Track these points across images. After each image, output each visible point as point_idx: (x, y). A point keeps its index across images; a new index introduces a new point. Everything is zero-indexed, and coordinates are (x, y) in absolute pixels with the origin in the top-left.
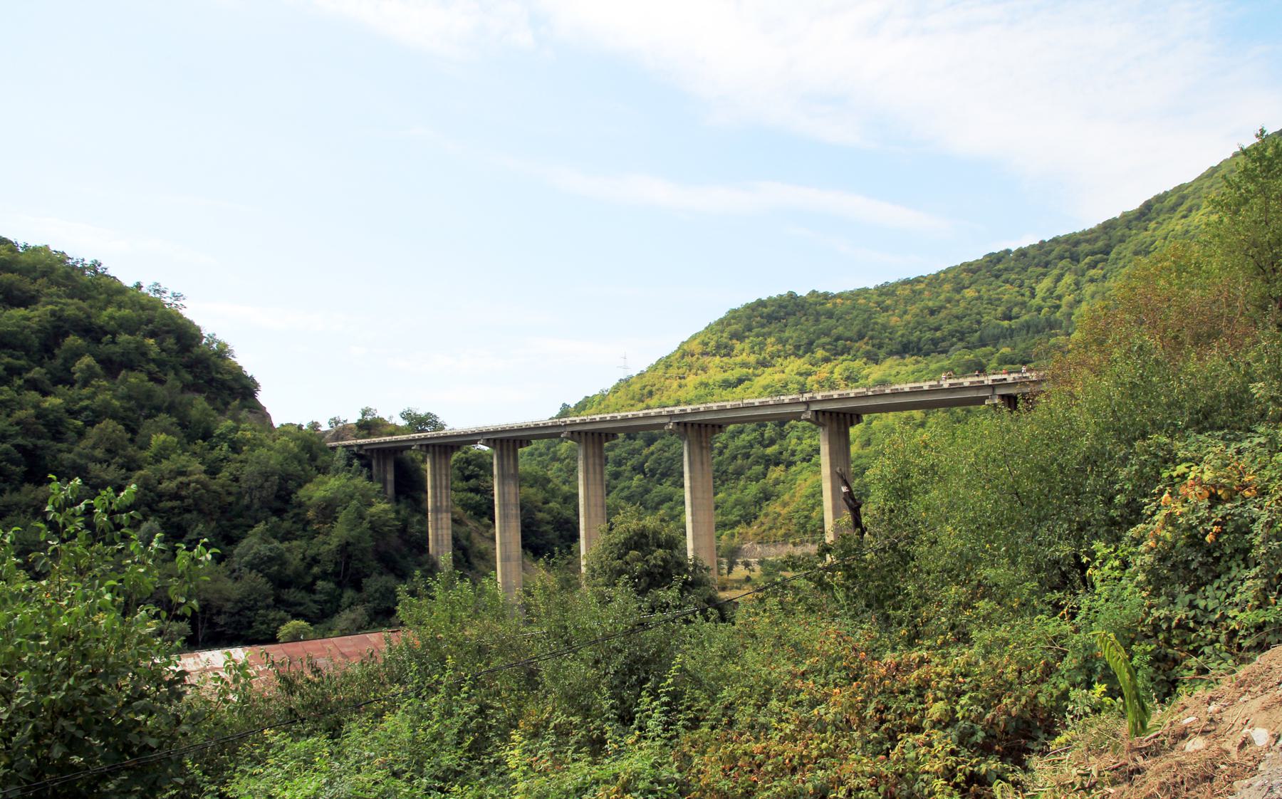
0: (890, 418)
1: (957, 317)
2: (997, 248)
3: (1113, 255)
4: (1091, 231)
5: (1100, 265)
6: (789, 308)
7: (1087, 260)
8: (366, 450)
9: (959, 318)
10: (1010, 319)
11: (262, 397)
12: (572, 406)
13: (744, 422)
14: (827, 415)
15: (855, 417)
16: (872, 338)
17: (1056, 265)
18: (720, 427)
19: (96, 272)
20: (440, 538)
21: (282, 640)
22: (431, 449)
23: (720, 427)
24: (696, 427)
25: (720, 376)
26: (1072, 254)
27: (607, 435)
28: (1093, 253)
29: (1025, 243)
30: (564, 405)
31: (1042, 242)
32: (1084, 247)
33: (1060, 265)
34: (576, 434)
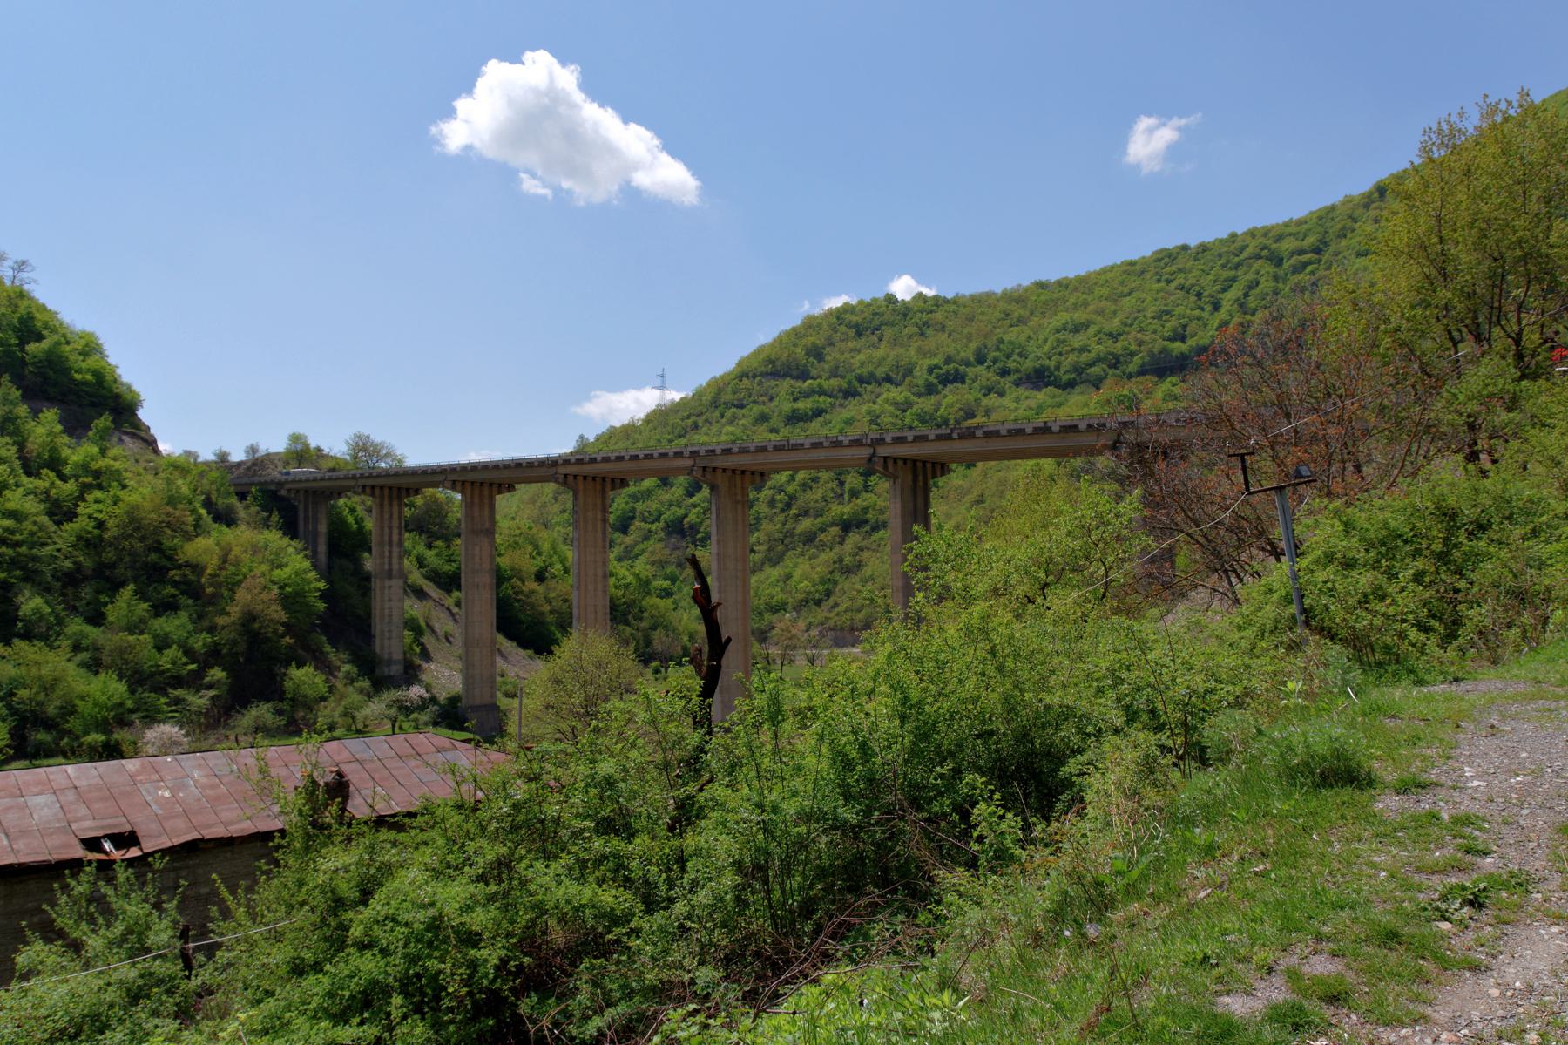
0: (1242, 478)
1: (1111, 335)
2: (1171, 243)
3: (1326, 257)
4: (1300, 222)
5: (1309, 269)
6: (885, 317)
7: (1292, 261)
8: (289, 490)
9: (1114, 337)
10: (1183, 339)
11: (142, 414)
12: (592, 440)
13: (818, 469)
14: (900, 463)
15: (938, 467)
16: (995, 361)
17: (1250, 266)
18: (762, 474)
19: (1387, 529)
20: (387, 611)
21: (150, 750)
22: (377, 491)
23: (762, 474)
24: (729, 473)
25: (787, 407)
26: (1272, 252)
27: (613, 480)
28: (1301, 252)
29: (1208, 237)
30: (582, 437)
31: (1233, 236)
32: (1287, 245)
33: (1256, 266)
34: (570, 479)
